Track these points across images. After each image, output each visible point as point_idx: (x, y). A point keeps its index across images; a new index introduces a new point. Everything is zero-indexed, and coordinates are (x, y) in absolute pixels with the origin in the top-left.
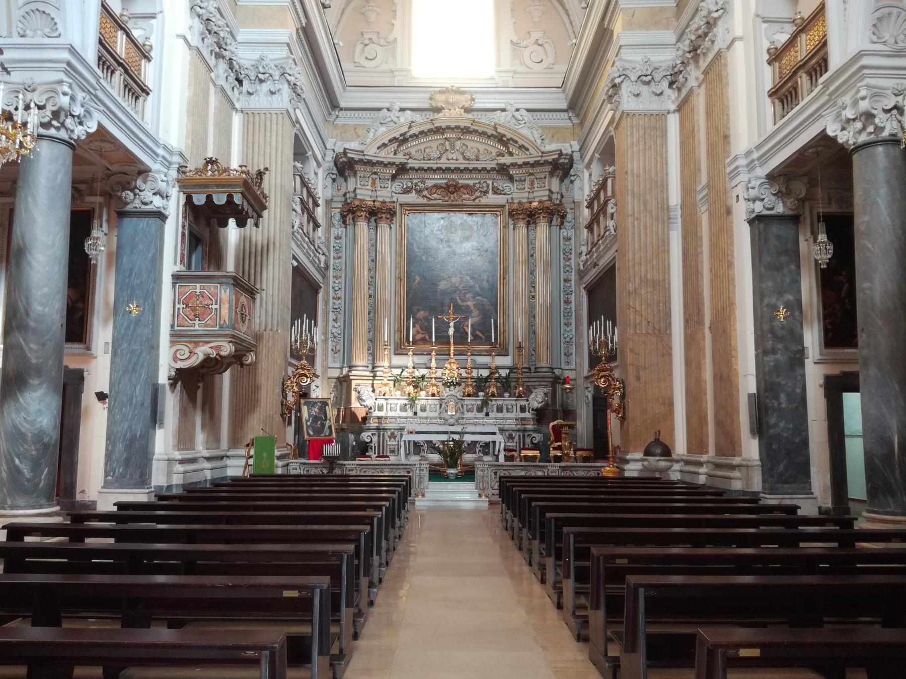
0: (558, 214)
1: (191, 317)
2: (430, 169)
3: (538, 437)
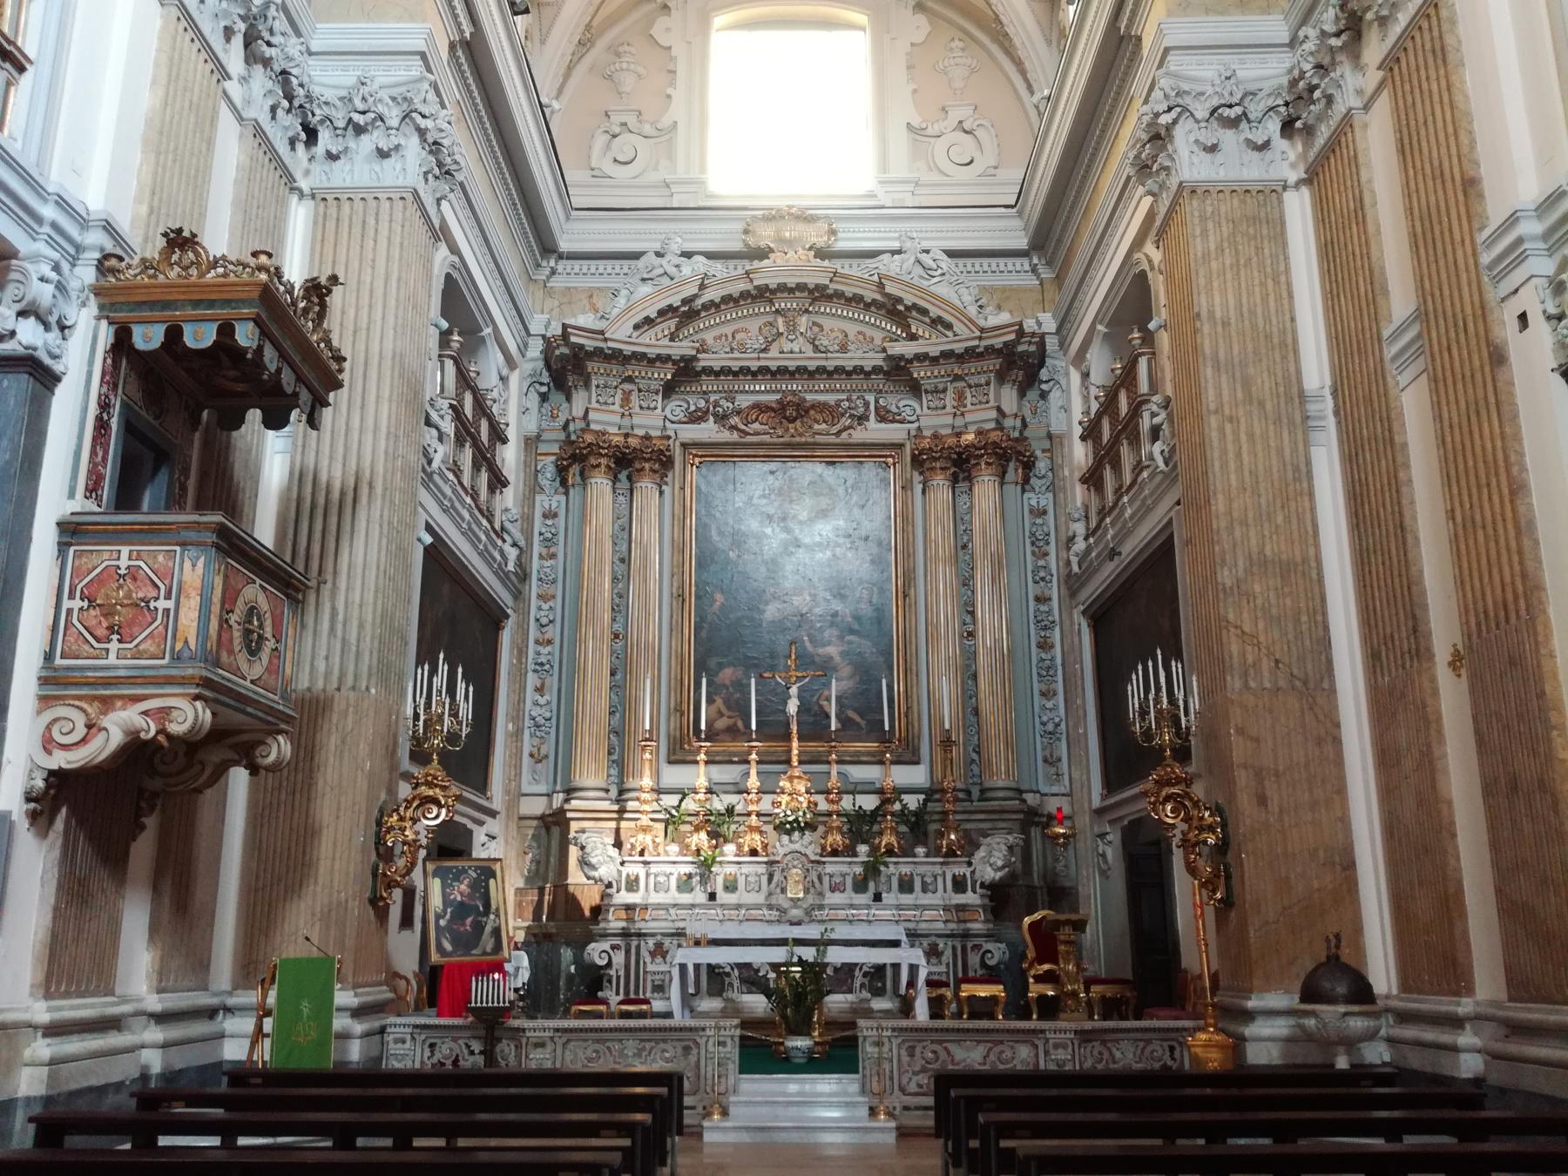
0: (1018, 460)
1: (101, 632)
2: (745, 371)
3: (997, 952)
